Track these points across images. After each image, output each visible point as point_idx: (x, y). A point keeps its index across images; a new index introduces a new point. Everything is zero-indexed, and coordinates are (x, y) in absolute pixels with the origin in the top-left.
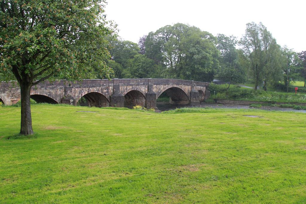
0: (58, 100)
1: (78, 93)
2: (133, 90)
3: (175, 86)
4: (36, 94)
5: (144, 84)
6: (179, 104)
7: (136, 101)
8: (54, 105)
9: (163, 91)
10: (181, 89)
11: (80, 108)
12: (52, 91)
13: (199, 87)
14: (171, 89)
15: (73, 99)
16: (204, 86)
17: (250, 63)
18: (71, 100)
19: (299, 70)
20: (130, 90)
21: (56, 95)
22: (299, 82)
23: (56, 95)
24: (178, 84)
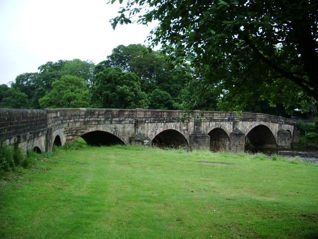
0: (126, 140)
1: (152, 130)
2: (217, 127)
3: (262, 123)
4: (99, 129)
5: (229, 120)
6: (264, 147)
7: (215, 143)
8: (110, 148)
9: (250, 130)
10: (268, 126)
11: (159, 151)
12: (118, 126)
13: (287, 125)
14: (256, 128)
15: (148, 140)
16: (292, 125)
17: (184, 42)
18: (145, 141)
19: (108, 62)
20: (213, 128)
21: (124, 133)
22: (260, 155)
23: (124, 133)
24: (265, 121)
